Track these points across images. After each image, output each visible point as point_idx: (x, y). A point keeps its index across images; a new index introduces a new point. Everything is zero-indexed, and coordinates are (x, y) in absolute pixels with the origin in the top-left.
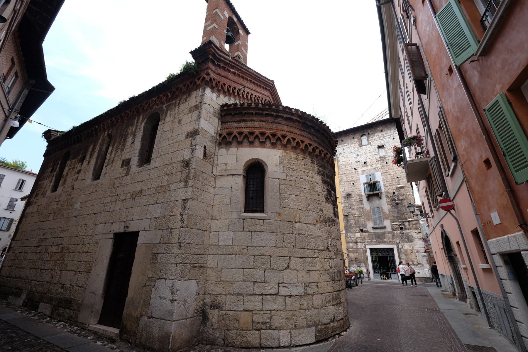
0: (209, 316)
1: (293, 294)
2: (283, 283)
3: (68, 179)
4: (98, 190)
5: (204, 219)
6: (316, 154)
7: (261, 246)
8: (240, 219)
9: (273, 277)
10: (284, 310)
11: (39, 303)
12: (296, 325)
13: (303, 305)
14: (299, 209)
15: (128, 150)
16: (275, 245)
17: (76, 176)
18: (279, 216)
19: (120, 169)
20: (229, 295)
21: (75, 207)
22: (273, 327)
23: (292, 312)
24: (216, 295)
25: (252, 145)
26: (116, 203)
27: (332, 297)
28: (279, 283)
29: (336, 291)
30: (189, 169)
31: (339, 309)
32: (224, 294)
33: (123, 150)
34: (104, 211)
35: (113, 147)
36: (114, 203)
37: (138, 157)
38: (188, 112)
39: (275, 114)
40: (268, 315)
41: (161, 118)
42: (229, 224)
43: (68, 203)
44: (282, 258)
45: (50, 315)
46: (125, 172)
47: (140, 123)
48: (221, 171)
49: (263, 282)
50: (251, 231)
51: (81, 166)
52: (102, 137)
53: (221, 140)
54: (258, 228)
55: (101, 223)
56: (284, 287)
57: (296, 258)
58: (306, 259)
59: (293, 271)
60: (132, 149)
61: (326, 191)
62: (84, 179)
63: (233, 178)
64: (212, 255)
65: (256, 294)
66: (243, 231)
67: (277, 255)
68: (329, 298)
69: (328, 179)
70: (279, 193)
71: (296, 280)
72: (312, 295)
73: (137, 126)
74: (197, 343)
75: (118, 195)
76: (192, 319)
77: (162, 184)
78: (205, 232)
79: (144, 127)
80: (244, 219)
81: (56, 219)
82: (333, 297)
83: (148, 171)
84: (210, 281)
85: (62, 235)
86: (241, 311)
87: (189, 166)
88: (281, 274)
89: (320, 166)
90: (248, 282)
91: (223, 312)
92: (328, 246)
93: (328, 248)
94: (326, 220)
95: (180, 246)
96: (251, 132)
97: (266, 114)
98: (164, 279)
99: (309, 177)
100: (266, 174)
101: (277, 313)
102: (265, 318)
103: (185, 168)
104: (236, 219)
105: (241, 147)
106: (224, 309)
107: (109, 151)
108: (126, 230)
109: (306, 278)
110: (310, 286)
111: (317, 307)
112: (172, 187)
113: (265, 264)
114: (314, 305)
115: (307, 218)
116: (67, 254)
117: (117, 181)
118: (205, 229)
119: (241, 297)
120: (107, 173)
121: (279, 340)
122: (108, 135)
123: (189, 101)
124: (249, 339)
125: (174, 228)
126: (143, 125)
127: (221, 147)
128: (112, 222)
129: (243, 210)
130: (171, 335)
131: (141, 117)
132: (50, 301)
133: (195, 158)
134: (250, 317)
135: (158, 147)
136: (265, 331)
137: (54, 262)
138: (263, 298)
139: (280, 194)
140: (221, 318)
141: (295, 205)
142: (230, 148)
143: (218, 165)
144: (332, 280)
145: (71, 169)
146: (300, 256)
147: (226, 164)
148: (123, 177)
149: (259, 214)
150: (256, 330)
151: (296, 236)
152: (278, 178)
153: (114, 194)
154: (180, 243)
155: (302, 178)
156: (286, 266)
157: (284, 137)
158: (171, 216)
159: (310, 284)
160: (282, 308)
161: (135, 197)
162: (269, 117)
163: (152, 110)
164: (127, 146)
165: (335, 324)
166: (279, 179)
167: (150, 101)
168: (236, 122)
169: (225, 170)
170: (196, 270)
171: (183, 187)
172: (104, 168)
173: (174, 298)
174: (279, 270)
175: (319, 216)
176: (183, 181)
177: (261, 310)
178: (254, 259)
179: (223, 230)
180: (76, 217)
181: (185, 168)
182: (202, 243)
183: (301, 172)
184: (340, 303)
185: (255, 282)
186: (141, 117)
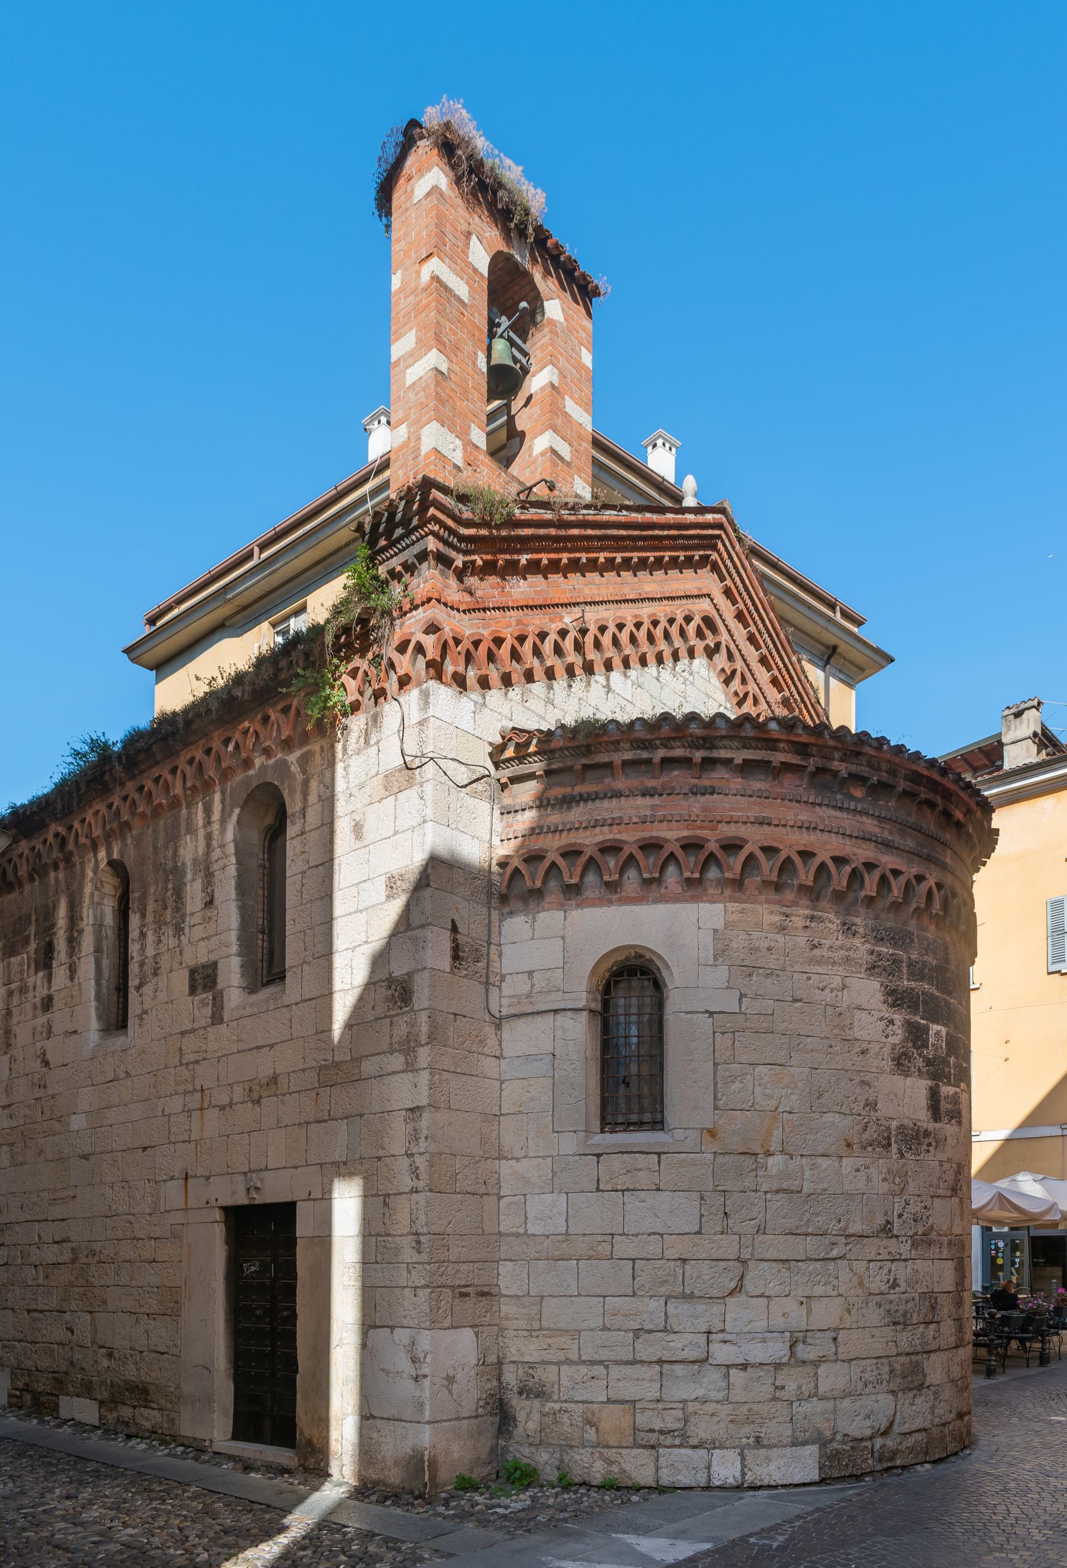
0: (517, 1415)
1: (752, 1360)
2: (723, 1331)
3: (16, 1029)
4: (133, 1072)
5: (478, 1162)
6: (862, 894)
7: (654, 1234)
8: (587, 1155)
9: (692, 1316)
10: (726, 1400)
11: (57, 1396)
12: (759, 1437)
13: (783, 1388)
14: (781, 1109)
15: (198, 932)
16: (696, 1228)
17: (42, 1019)
18: (710, 1139)
19: (190, 999)
20: (568, 1364)
21: (74, 1127)
22: (694, 1441)
23: (747, 1406)
24: (532, 1365)
25: (615, 897)
26: (202, 1115)
27: (886, 1369)
28: (709, 1332)
29: (907, 1354)
30: (412, 1010)
31: (912, 1404)
32: (552, 1363)
33: (182, 929)
34: (172, 1139)
35: (143, 916)
36: (196, 1115)
37: (239, 959)
38: (382, 792)
39: (698, 755)
40: (676, 1411)
41: (289, 811)
42: (553, 1171)
43: (45, 1112)
44: (721, 1263)
45: (97, 1424)
46: (208, 1011)
47: (216, 827)
48: (515, 1000)
49: (661, 1331)
50: (623, 1191)
51: (50, 981)
52: (90, 874)
53: (505, 884)
54: (644, 1179)
55: (172, 1178)
56: (725, 1342)
57: (766, 1264)
58: (800, 1264)
59: (754, 1299)
60: (211, 929)
61: (899, 1032)
62: (75, 1032)
63: (558, 1023)
64: (511, 1260)
65: (642, 1362)
66: (598, 1190)
67: (703, 1256)
68: (876, 1373)
69: (913, 984)
70: (711, 1063)
71: (762, 1324)
72: (816, 1363)
73: (209, 837)
74: (494, 1476)
75: (202, 1090)
76: (472, 1421)
77: (336, 1059)
78: (485, 1197)
79: (234, 841)
80: (598, 1156)
81: (22, 1164)
82: (891, 1371)
83: (284, 1010)
84: (512, 1332)
85: (58, 1212)
86: (603, 1402)
87: (411, 1000)
88: (717, 1309)
89: (882, 939)
90: (619, 1330)
91: (553, 1405)
92: (888, 1222)
93: (886, 1230)
94: (889, 1138)
95: (419, 1242)
96: (609, 844)
97: (665, 761)
98: (387, 1327)
99: (827, 991)
100: (668, 998)
101: (703, 1407)
102: (667, 1418)
103: (401, 1008)
104: (574, 1155)
105: (579, 906)
106: (555, 1397)
107: (134, 933)
108: (254, 1199)
109: (797, 1318)
110: (809, 1340)
111: (829, 1395)
112: (369, 1067)
113: (666, 1281)
114: (821, 1390)
115: (813, 1137)
116: (93, 1269)
117: (189, 1042)
118: (482, 1189)
119: (600, 1370)
120: (145, 1012)
121: (709, 1472)
122: (111, 863)
123: (377, 743)
124: (627, 1467)
125: (395, 1194)
126: (230, 834)
127: (506, 910)
128: (208, 1174)
129: (596, 1123)
130: (426, 1453)
131: (217, 797)
132: (87, 1389)
133: (426, 974)
134: (629, 1418)
135: (299, 927)
136: (669, 1450)
137: (60, 1289)
138: (664, 1371)
139: (716, 1065)
140: (549, 1420)
141: (769, 1097)
142: (538, 912)
143: (503, 978)
144: (895, 1324)
145: (16, 994)
146: (785, 1258)
147: (530, 973)
148: (205, 1028)
149: (649, 1133)
150: (644, 1447)
151: (769, 1196)
152: (707, 1012)
153: (191, 1088)
154: (417, 1234)
155: (800, 1000)
156: (733, 1285)
157: (732, 847)
158: (379, 1158)
159: (809, 1334)
160: (720, 1395)
161: (261, 1097)
162: (676, 773)
163: (251, 772)
164: (192, 914)
165: (890, 1443)
166: (711, 1014)
167: (237, 736)
168: (553, 806)
169: (529, 996)
170: (470, 1302)
171: (401, 1068)
172: (132, 994)
173: (420, 1372)
174: (710, 1298)
175: (859, 1128)
176: (399, 1051)
177: (658, 1401)
178: (633, 1268)
179: (537, 1191)
180: (85, 1157)
181: (401, 1008)
182: (480, 1231)
183: (796, 976)
184: (921, 1386)
185: (637, 1333)
186: (217, 797)
